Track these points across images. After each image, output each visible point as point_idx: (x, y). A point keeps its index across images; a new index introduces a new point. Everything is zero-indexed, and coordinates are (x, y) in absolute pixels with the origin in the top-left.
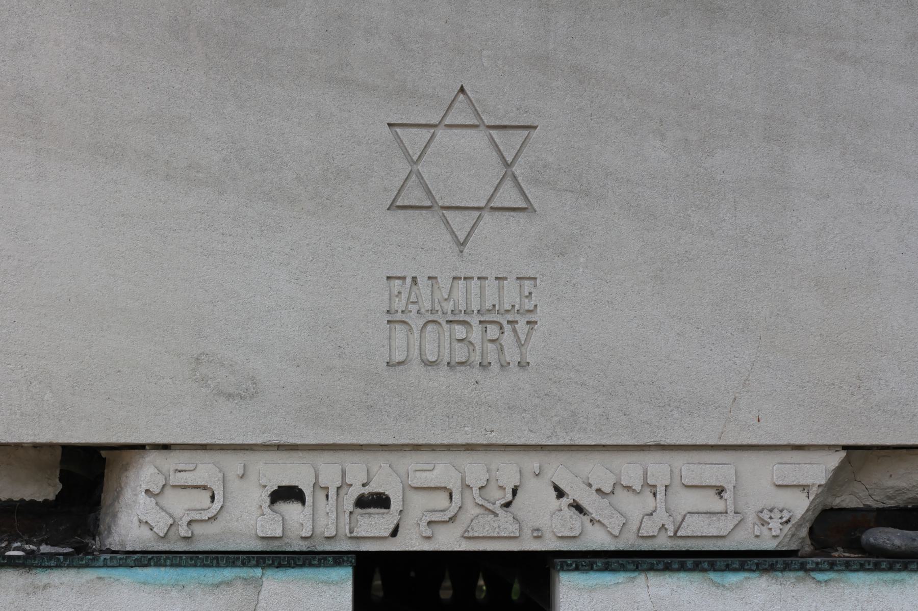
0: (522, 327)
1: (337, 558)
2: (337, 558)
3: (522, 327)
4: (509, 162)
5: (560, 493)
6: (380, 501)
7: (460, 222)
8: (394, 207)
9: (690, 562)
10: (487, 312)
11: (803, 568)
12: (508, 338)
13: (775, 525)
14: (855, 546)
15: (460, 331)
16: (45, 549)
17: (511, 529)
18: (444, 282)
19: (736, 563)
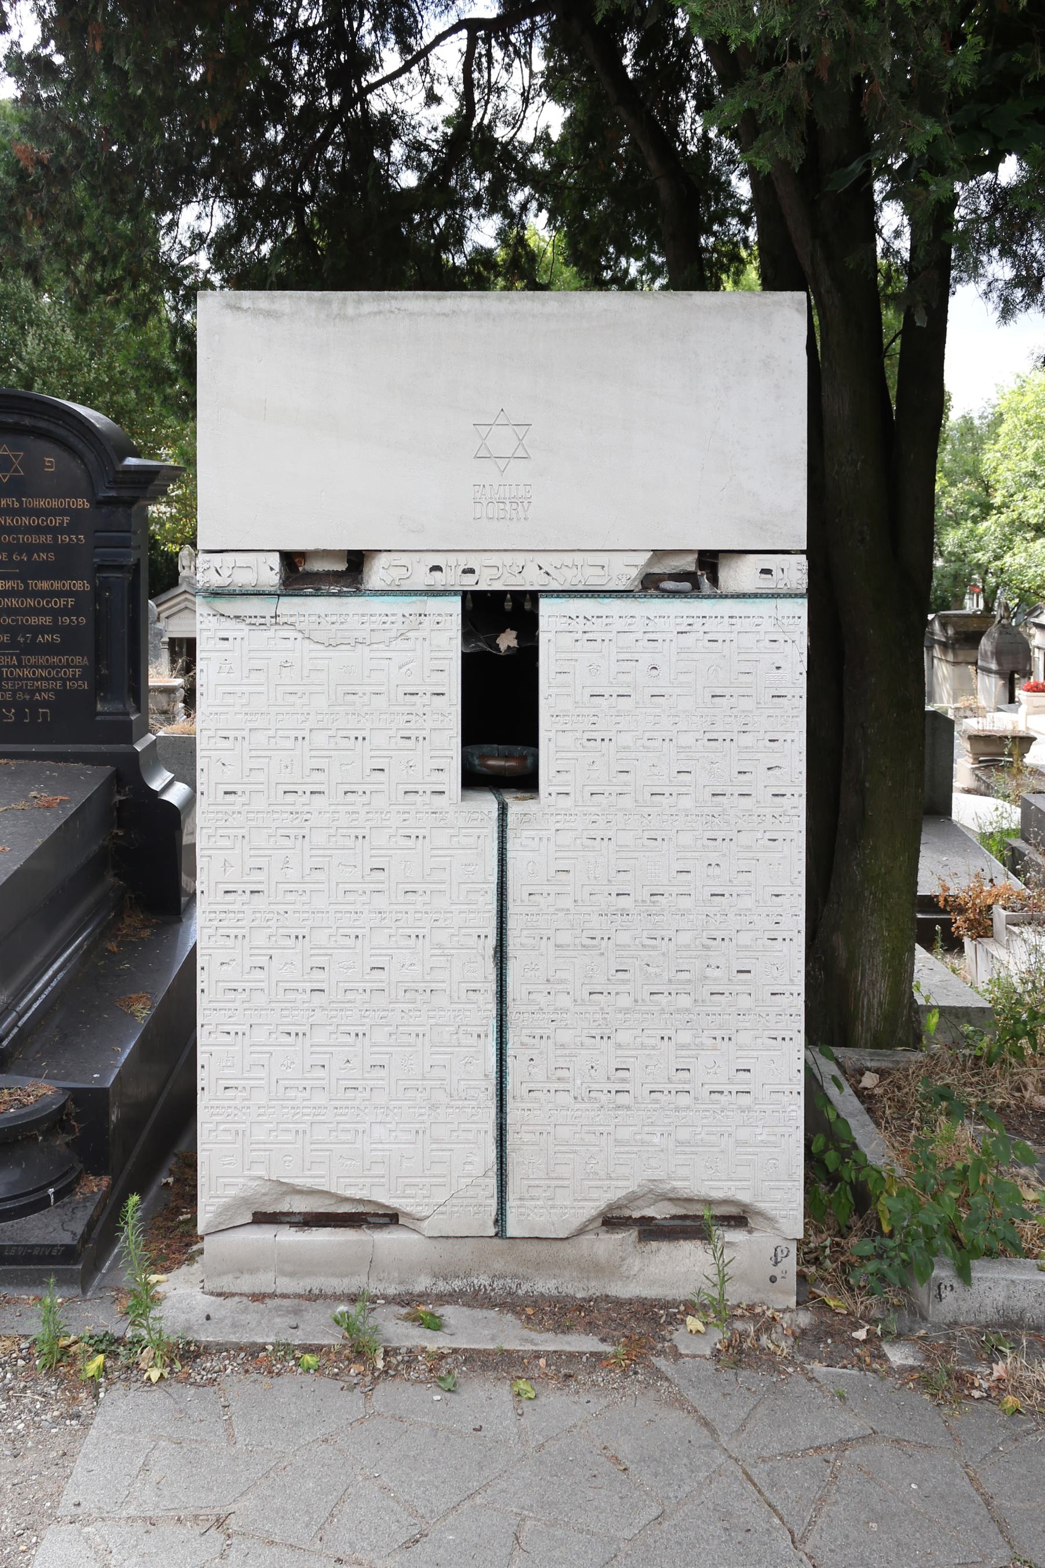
0: (526, 504)
1: (455, 593)
2: (455, 593)
3: (526, 504)
4: (464, 33)
5: (541, 568)
6: (471, 571)
7: (502, 463)
8: (476, 457)
9: (590, 594)
10: (714, 1222)
11: (634, 597)
12: (520, 508)
13: (624, 580)
14: (657, 588)
15: (502, 506)
16: (345, 589)
17: (522, 582)
18: (496, 487)
19: (608, 594)
